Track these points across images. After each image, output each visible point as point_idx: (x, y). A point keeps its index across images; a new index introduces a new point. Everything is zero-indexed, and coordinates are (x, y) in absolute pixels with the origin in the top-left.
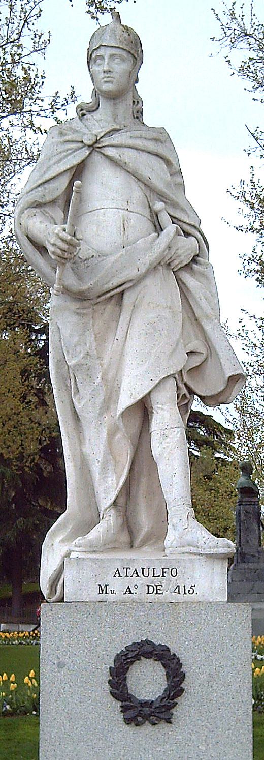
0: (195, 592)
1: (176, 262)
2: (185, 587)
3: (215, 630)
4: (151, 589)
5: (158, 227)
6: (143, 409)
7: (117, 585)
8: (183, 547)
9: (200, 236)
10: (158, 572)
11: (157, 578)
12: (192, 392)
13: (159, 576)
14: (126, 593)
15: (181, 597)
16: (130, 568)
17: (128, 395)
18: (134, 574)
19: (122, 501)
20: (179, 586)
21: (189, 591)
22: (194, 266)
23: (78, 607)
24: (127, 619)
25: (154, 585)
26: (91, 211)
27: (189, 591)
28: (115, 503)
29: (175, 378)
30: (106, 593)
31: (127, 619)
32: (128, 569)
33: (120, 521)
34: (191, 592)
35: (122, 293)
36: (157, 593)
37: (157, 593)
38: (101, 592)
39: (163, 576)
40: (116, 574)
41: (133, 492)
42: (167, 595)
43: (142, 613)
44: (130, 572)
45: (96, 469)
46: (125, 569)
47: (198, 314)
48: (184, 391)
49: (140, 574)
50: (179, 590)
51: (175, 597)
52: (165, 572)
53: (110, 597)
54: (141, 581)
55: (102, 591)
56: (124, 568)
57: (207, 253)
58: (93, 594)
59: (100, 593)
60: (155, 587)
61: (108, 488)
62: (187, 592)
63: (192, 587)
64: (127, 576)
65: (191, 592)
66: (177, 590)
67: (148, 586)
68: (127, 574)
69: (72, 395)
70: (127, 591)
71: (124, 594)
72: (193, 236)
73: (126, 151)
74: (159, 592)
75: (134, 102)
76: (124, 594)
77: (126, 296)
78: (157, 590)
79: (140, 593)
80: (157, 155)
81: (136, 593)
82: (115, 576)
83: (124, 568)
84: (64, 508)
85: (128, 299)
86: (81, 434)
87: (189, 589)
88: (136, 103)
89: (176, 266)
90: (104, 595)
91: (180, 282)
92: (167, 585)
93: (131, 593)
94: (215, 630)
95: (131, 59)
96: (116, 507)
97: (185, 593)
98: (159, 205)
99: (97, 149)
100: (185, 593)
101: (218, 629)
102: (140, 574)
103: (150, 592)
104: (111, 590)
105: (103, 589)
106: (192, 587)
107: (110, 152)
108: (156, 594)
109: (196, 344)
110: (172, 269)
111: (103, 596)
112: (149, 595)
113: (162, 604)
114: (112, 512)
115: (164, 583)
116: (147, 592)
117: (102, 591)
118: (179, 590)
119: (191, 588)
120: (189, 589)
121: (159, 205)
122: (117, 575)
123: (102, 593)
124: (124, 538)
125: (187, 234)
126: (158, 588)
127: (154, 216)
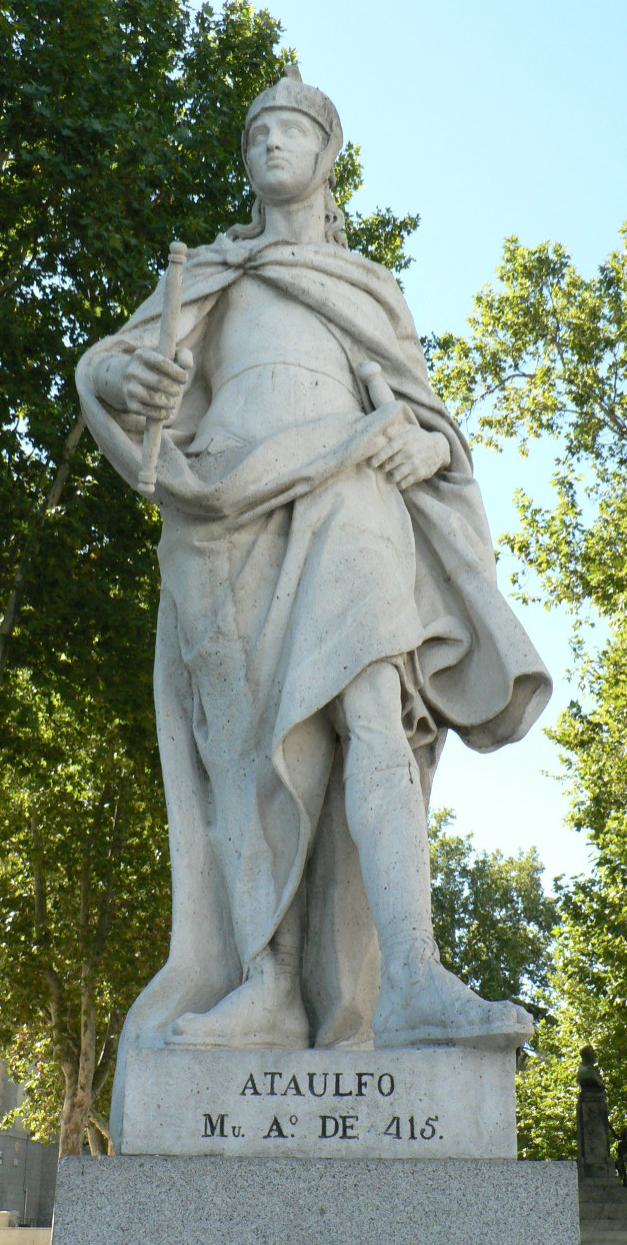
0: (437, 1135)
1: (405, 470)
2: (412, 1121)
3: (486, 1230)
4: (330, 1125)
5: (367, 404)
6: (331, 726)
7: (249, 1116)
8: (413, 1028)
9: (451, 431)
10: (349, 1084)
11: (345, 1098)
12: (443, 722)
13: (350, 1093)
14: (269, 1136)
15: (404, 1148)
16: (280, 1074)
17: (303, 697)
18: (288, 1087)
19: (288, 941)
20: (398, 1119)
21: (423, 1131)
22: (443, 485)
23: (147, 1167)
24: (265, 1199)
25: (337, 1116)
26: (236, 376)
27: (423, 1131)
28: (273, 944)
29: (397, 667)
30: (222, 1134)
31: (265, 1199)
32: (277, 1077)
33: (285, 984)
34: (428, 1133)
35: (290, 507)
36: (344, 1136)
37: (344, 1136)
38: (209, 1132)
39: (360, 1094)
40: (245, 1088)
41: (314, 922)
42: (367, 1136)
43: (302, 1185)
44: (281, 1084)
45: (240, 888)
46: (269, 1076)
47: (450, 563)
48: (421, 711)
49: (304, 1086)
50: (398, 1128)
51: (388, 1147)
52: (365, 1084)
53: (231, 1145)
54: (306, 1108)
55: (213, 1129)
56: (266, 1074)
57: (469, 467)
58: (188, 1137)
59: (206, 1136)
60: (340, 1121)
61: (260, 907)
62: (417, 1133)
63: (430, 1122)
64: (272, 1093)
65: (428, 1133)
66: (393, 1130)
67: (324, 1119)
68: (272, 1088)
69: (194, 724)
70: (271, 1130)
71: (265, 1137)
72: (439, 431)
73: (304, 272)
74: (350, 1132)
75: (327, 217)
76: (265, 1137)
77: (299, 509)
78: (344, 1128)
79: (303, 1135)
80: (370, 292)
81: (293, 1136)
82: (243, 1093)
83: (266, 1074)
84: (158, 949)
85: (306, 517)
86: (210, 806)
87: (424, 1126)
88: (332, 219)
89: (405, 477)
90: (216, 1138)
91: (417, 514)
92: (370, 1114)
93: (281, 1134)
94: (486, 1230)
95: (320, 134)
96: (275, 955)
97: (413, 1137)
98: (372, 368)
99: (252, 272)
100: (413, 1137)
101: (494, 1228)
102: (304, 1086)
103: (328, 1134)
104: (234, 1128)
105: (215, 1125)
106: (430, 1122)
107: (271, 272)
108: (341, 1138)
109: (443, 625)
110: (398, 484)
111: (215, 1143)
112: (324, 1139)
113: (354, 1162)
114: (268, 966)
115: (363, 1111)
116: (320, 1133)
117: (213, 1129)
118: (398, 1128)
119: (427, 1124)
120: (424, 1126)
121: (372, 368)
122: (249, 1092)
123: (213, 1134)
124: (295, 1023)
125: (428, 427)
126: (349, 1122)
127: (361, 387)
